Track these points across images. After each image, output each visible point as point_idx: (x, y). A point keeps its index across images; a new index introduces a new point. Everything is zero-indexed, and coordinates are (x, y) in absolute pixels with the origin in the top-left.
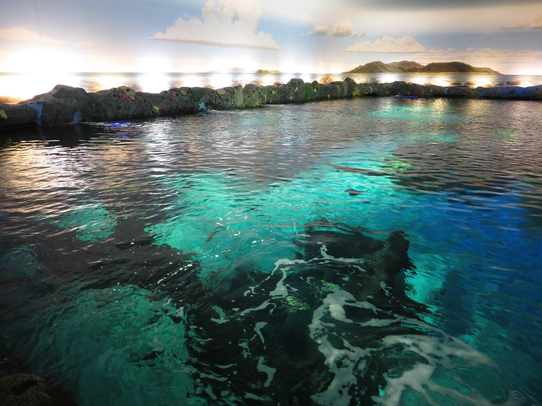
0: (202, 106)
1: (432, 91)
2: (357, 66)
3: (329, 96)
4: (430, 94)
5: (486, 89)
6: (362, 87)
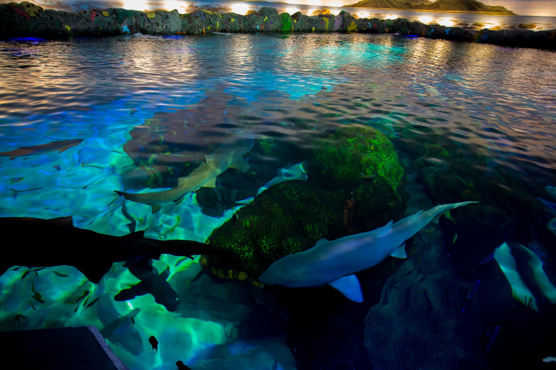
0: (125, 28)
1: (433, 30)
3: (314, 29)
5: (491, 31)
6: (361, 22)
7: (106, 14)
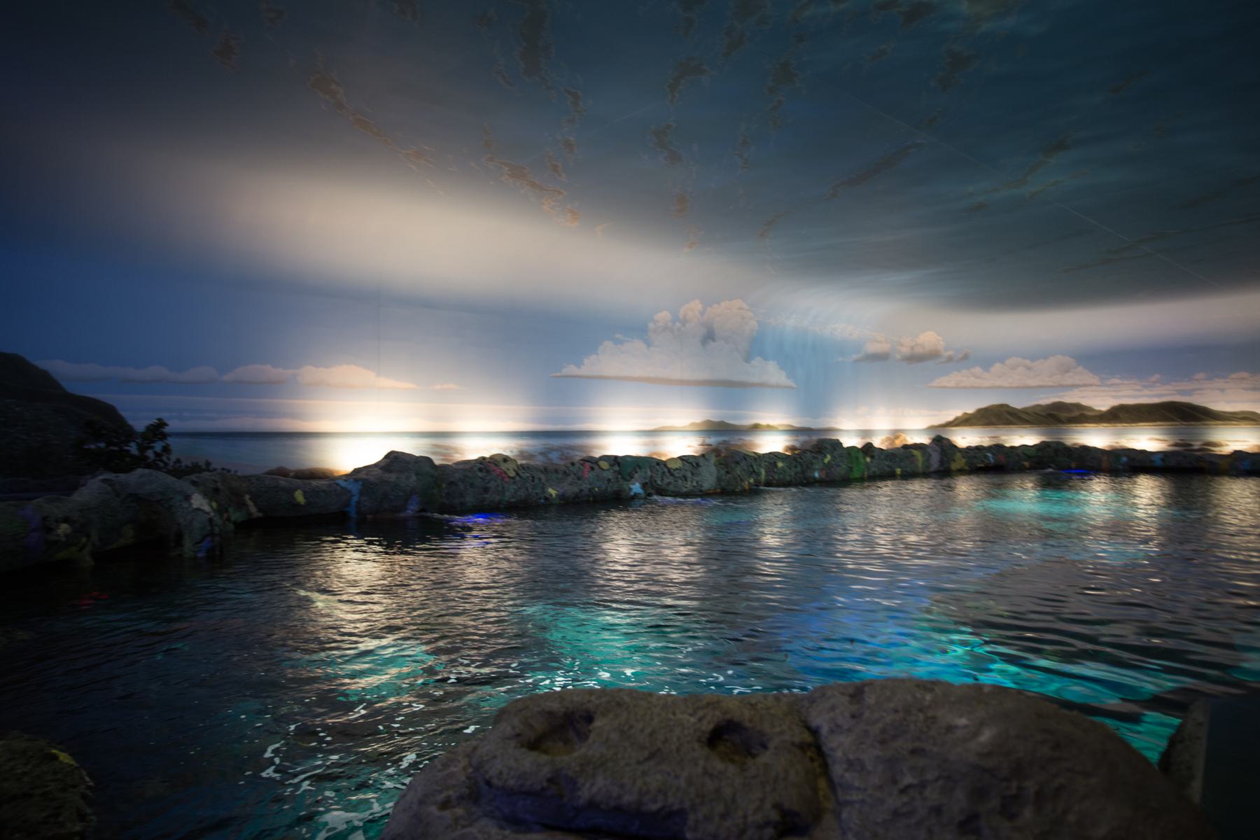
0: (636, 488)
2: (959, 413)
3: (898, 471)
4: (1126, 465)
7: (604, 465)
